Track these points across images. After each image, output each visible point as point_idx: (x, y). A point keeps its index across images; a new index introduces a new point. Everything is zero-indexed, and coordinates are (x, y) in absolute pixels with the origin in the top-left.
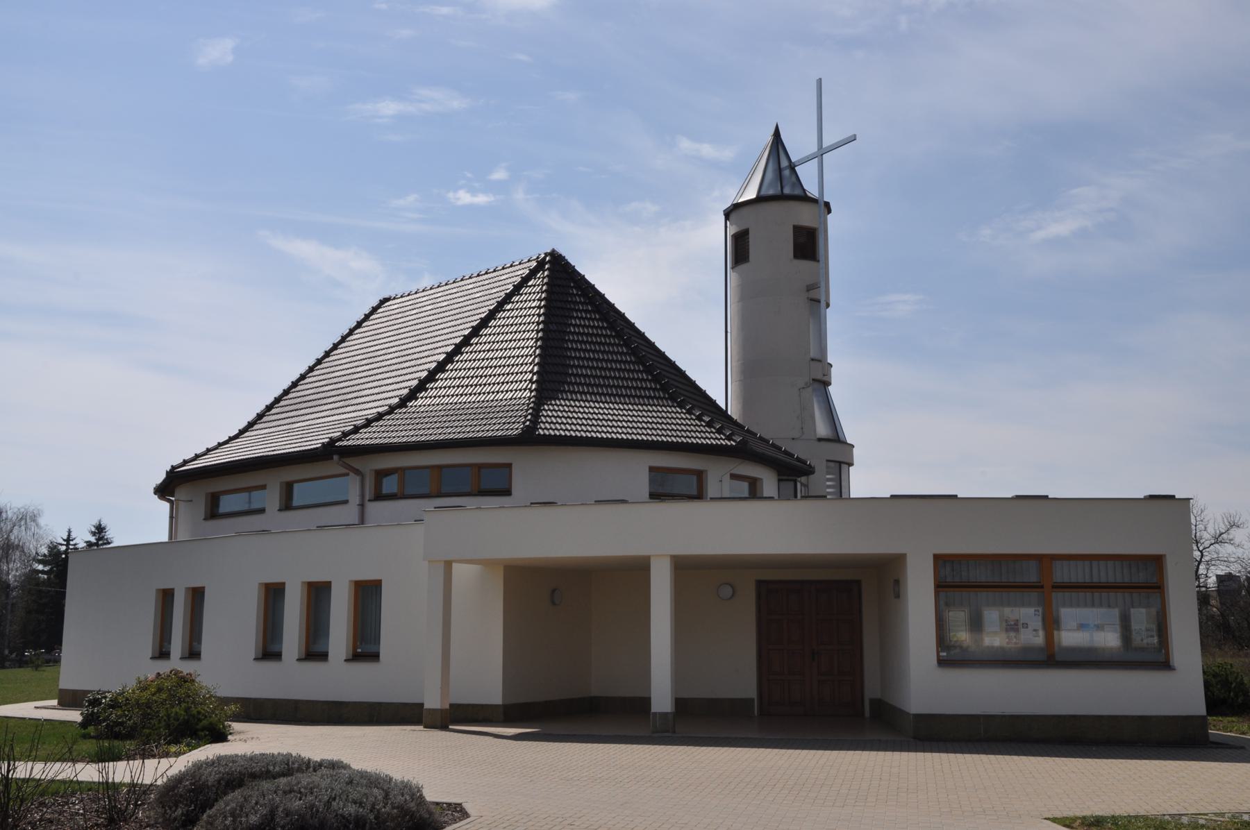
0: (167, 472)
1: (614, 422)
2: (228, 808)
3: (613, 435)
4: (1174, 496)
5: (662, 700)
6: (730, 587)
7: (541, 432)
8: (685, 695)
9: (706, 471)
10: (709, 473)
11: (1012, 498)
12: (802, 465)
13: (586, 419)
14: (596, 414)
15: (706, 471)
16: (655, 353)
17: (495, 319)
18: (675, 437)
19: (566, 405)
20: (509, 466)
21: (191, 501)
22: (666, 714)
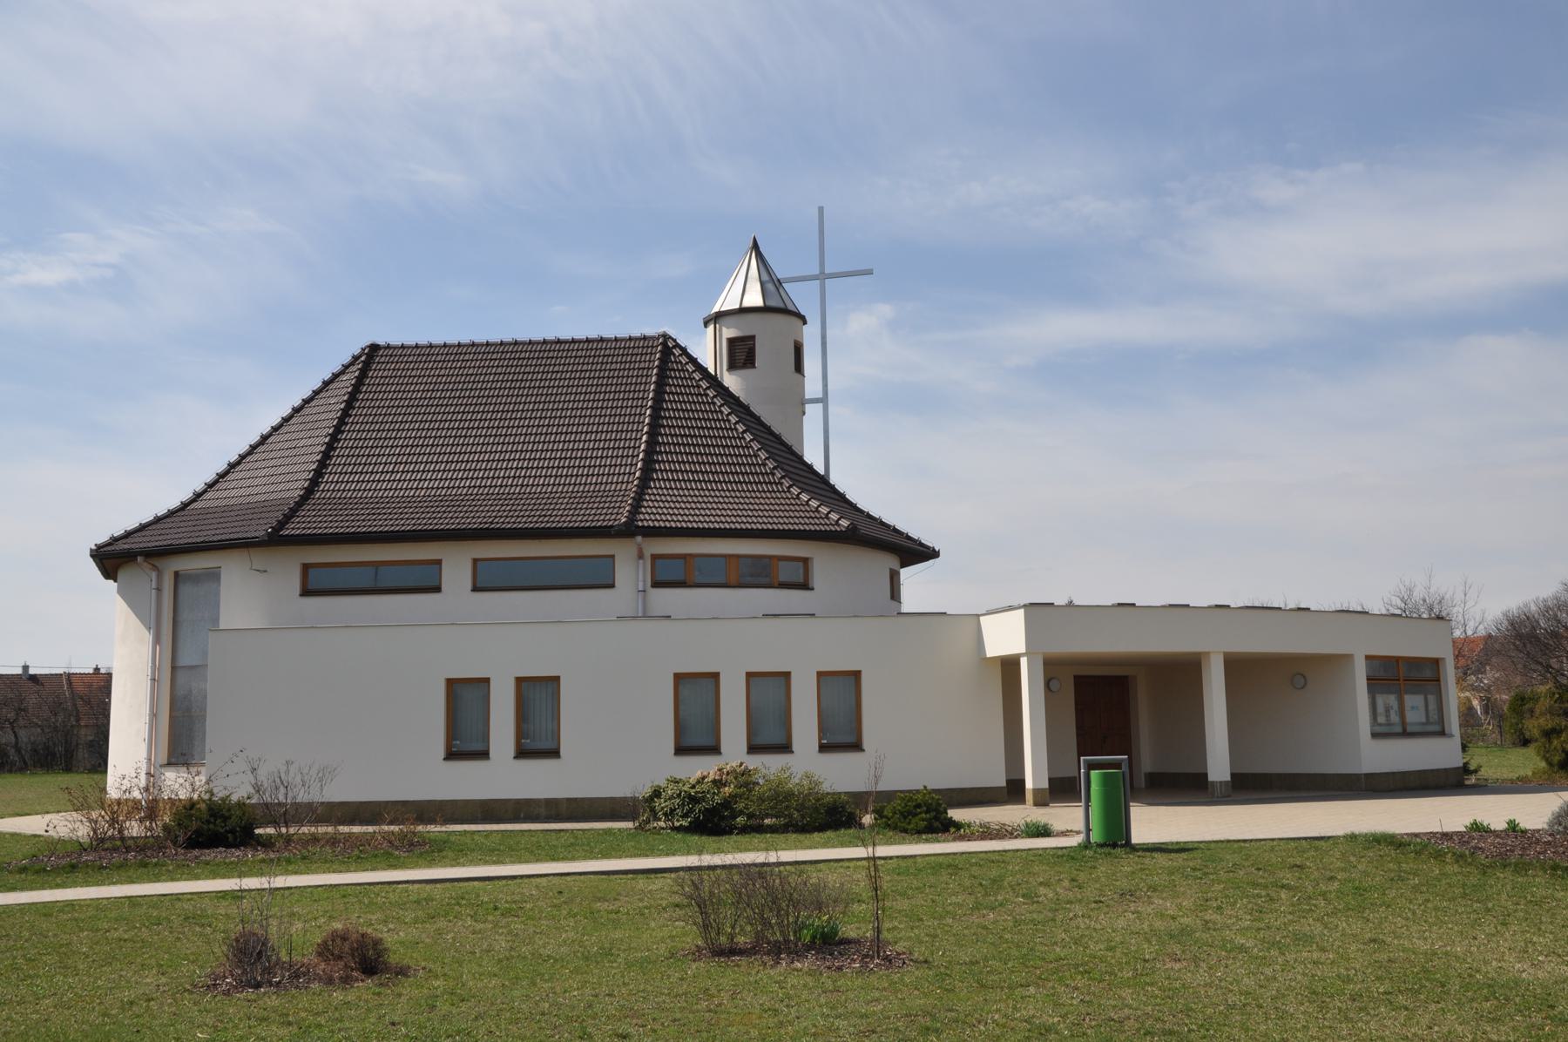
0: (91, 550)
1: (739, 512)
2: (248, 801)
3: (790, 526)
4: (1053, 604)
5: (1219, 768)
6: (1051, 684)
7: (640, 524)
8: (1052, 776)
9: (812, 558)
10: (815, 560)
11: (1113, 606)
12: (925, 550)
13: (752, 510)
14: (742, 504)
15: (812, 558)
16: (774, 439)
17: (354, 409)
18: (823, 525)
19: (752, 497)
20: (613, 557)
21: (265, 571)
22: (1228, 781)
